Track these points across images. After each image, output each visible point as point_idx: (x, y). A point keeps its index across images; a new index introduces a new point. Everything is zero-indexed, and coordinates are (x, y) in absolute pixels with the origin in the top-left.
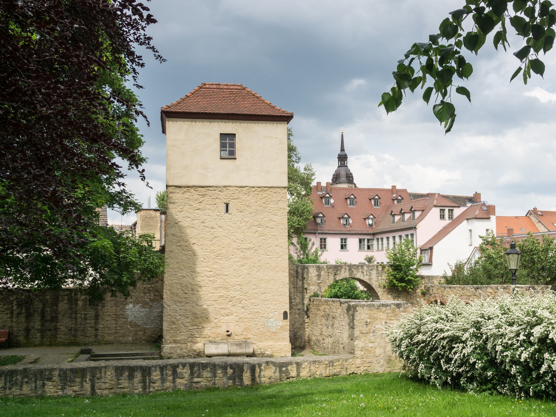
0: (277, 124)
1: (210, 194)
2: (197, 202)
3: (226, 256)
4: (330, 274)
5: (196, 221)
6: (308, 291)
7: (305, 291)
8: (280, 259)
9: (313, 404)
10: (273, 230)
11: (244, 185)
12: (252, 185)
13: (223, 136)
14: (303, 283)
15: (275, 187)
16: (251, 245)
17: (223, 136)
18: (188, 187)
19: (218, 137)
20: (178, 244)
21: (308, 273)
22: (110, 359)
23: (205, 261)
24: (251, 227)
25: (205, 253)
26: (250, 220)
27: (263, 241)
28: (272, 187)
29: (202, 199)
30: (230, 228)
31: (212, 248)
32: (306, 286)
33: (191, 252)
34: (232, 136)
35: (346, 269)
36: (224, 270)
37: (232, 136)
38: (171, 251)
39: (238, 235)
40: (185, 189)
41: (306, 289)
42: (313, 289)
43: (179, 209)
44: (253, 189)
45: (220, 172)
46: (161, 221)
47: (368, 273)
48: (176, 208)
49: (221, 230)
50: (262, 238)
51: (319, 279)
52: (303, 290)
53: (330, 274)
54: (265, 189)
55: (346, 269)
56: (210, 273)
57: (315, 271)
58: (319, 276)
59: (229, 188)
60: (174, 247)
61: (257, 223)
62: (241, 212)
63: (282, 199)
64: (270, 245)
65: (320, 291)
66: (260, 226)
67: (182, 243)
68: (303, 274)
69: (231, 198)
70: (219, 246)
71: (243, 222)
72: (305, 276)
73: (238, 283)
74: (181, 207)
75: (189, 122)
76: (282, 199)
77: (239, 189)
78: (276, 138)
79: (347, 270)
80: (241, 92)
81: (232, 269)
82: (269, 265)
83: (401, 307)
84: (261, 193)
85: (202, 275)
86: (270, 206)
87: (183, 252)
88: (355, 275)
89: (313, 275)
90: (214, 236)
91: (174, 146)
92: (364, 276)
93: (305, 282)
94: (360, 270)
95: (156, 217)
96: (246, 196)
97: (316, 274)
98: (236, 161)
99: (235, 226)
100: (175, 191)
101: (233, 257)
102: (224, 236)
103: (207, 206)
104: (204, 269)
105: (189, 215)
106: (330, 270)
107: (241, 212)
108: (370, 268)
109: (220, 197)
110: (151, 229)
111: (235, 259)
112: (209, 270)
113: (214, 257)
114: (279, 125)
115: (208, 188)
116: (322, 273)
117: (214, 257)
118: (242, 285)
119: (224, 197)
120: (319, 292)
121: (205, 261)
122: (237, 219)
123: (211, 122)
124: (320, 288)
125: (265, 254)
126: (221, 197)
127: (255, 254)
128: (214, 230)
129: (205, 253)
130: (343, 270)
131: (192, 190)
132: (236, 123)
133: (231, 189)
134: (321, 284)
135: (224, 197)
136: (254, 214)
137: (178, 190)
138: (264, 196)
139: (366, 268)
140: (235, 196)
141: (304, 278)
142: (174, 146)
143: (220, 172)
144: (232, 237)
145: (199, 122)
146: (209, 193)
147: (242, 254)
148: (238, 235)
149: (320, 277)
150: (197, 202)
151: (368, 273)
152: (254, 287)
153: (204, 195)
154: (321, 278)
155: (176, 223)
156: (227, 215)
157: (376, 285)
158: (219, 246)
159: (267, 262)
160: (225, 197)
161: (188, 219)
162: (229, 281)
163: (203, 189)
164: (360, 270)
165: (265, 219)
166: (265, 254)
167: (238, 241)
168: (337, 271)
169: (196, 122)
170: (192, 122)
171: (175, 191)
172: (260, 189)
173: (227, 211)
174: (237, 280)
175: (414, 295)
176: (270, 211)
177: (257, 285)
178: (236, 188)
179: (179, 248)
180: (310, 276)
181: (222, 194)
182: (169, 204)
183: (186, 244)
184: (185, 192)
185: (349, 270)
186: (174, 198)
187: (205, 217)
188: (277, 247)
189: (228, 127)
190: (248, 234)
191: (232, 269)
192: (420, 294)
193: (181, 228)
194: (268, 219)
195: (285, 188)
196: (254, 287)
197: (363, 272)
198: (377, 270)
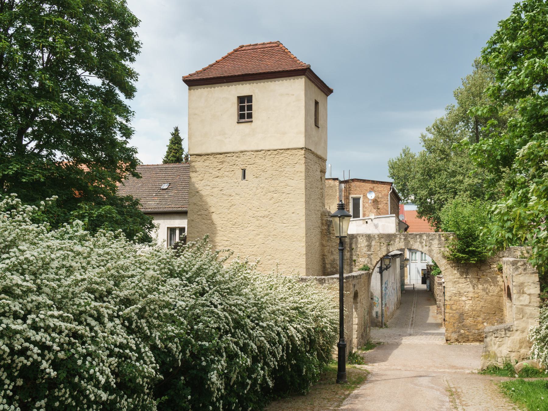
0: (294, 79)
1: (228, 160)
2: (216, 170)
3: (242, 225)
4: (382, 244)
5: (216, 189)
6: (357, 264)
7: (354, 263)
8: (297, 227)
9: (440, 399)
10: (290, 195)
11: (260, 149)
12: (267, 148)
13: (241, 99)
14: (351, 255)
15: (292, 149)
16: (267, 213)
17: (241, 99)
18: (208, 155)
19: (235, 101)
20: (198, 213)
21: (357, 243)
22: (430, 334)
23: (222, 230)
24: (266, 193)
25: (222, 222)
26: (266, 186)
27: (279, 208)
28: (288, 149)
29: (221, 166)
30: (247, 195)
31: (229, 216)
32: (354, 258)
33: (210, 221)
34: (249, 98)
35: (400, 239)
36: (240, 239)
37: (249, 98)
38: (193, 220)
39: (254, 202)
40: (205, 157)
41: (355, 261)
42: (362, 261)
43: (200, 178)
44: (269, 153)
45: (237, 137)
46: (341, 191)
47: (428, 244)
48: (197, 177)
49: (238, 197)
50: (277, 205)
51: (369, 250)
52: (351, 262)
53: (382, 244)
54: (281, 151)
55: (400, 239)
56: (227, 243)
57: (365, 241)
58: (369, 246)
59: (245, 153)
60: (195, 216)
61: (273, 189)
62: (257, 177)
63: (299, 162)
64: (286, 212)
65: (371, 264)
66: (275, 192)
67: (203, 212)
68: (351, 244)
69: (248, 163)
70: (235, 214)
71: (259, 188)
72: (354, 246)
73: (253, 253)
74: (202, 175)
75: (209, 89)
76: (299, 162)
77: (255, 154)
78: (293, 95)
79: (403, 240)
80: (276, 49)
81: (247, 239)
82: (285, 234)
83: (325, 282)
84: (277, 156)
85: (219, 245)
86: (287, 170)
87: (203, 221)
88: (412, 245)
89: (362, 245)
90: (231, 204)
91: (195, 114)
92: (422, 247)
93: (354, 254)
94: (418, 240)
95: (335, 186)
96: (262, 160)
97: (366, 244)
98: (253, 124)
99: (251, 192)
100: (196, 159)
101: (249, 225)
102: (240, 203)
103: (226, 173)
104: (222, 238)
105: (209, 183)
106: (382, 240)
107: (257, 177)
108: (430, 238)
109: (237, 163)
110: (330, 199)
111: (250, 228)
112: (226, 239)
113: (231, 226)
114: (296, 80)
115: (226, 155)
116: (373, 243)
117: (231, 226)
118: (257, 255)
119: (241, 162)
120: (369, 265)
121: (222, 230)
122: (253, 186)
123: (228, 86)
124: (371, 260)
125: (280, 222)
126: (239, 163)
127: (271, 222)
128: (232, 198)
129: (222, 222)
130: (397, 240)
131: (211, 157)
132: (253, 83)
133: (248, 153)
134: (372, 256)
135: (241, 162)
136: (270, 179)
137: (199, 158)
138: (280, 159)
139: (425, 237)
140: (252, 161)
141: (353, 249)
142: (195, 114)
143: (237, 137)
144: (249, 204)
145: (218, 87)
146: (228, 159)
147: (258, 222)
148: (254, 202)
149: (370, 248)
150: (216, 170)
151: (428, 244)
152: (269, 257)
153: (222, 162)
154: (372, 249)
155: (198, 192)
156: (244, 181)
157: (437, 258)
158: (235, 214)
159: (282, 231)
160: (242, 163)
161: (208, 188)
162: (244, 250)
163: (221, 156)
164: (418, 240)
165: (281, 184)
166: (280, 222)
167: (254, 209)
168: (390, 241)
169: (214, 88)
170: (211, 88)
171: (196, 159)
172: (276, 152)
173: (244, 178)
174: (252, 250)
175: (488, 271)
176: (287, 175)
177: (272, 255)
178: (253, 153)
179: (199, 217)
180: (359, 246)
181: (239, 160)
182: (191, 173)
183: (206, 213)
184: (205, 160)
185: (405, 239)
186: (196, 166)
187: (224, 184)
188: (293, 215)
189: (244, 89)
190: (264, 201)
191: (247, 239)
192: (496, 269)
193: (201, 197)
194: (284, 184)
195: (302, 149)
196: (269, 257)
197: (421, 243)
198: (440, 239)
